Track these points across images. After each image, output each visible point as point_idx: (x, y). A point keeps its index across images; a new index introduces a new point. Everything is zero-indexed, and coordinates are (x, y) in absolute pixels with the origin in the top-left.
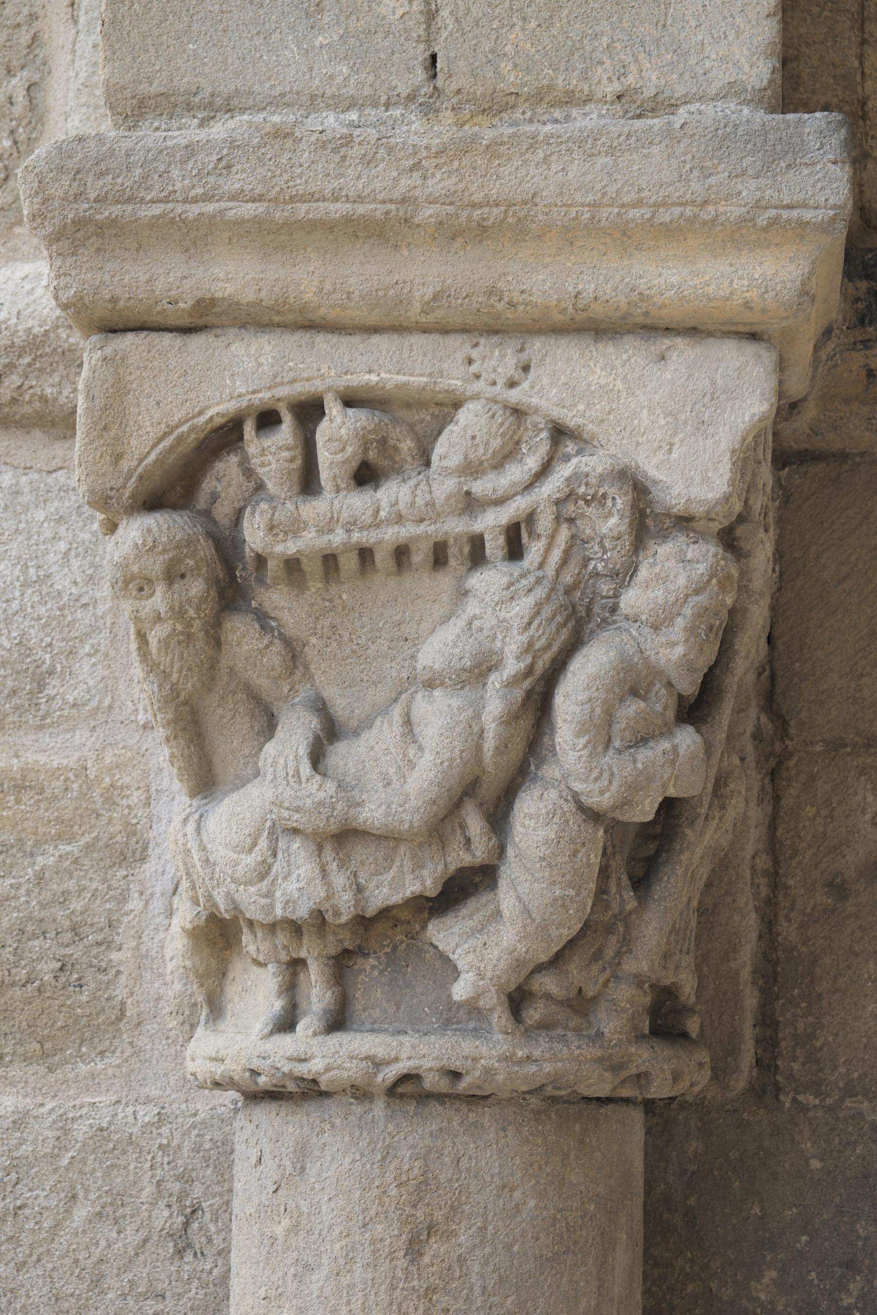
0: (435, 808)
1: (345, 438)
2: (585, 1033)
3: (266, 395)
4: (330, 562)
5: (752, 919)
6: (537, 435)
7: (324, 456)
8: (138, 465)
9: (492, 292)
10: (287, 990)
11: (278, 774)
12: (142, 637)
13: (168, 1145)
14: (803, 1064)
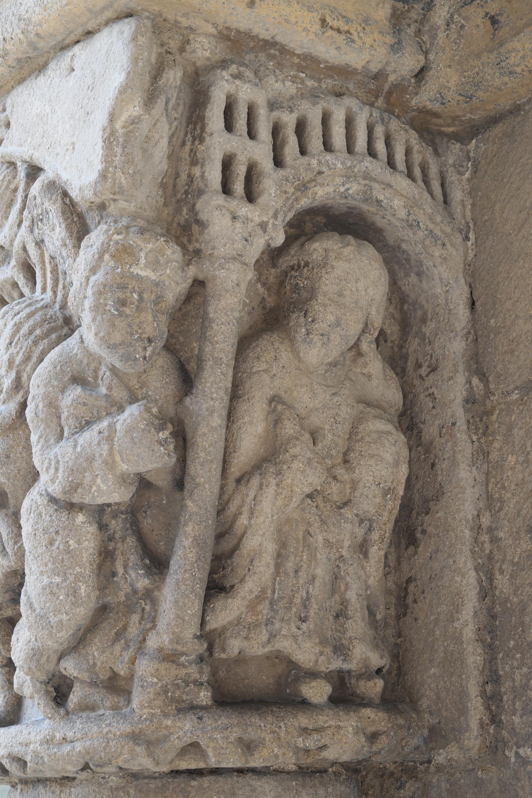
5: (472, 577)
14: (521, 717)
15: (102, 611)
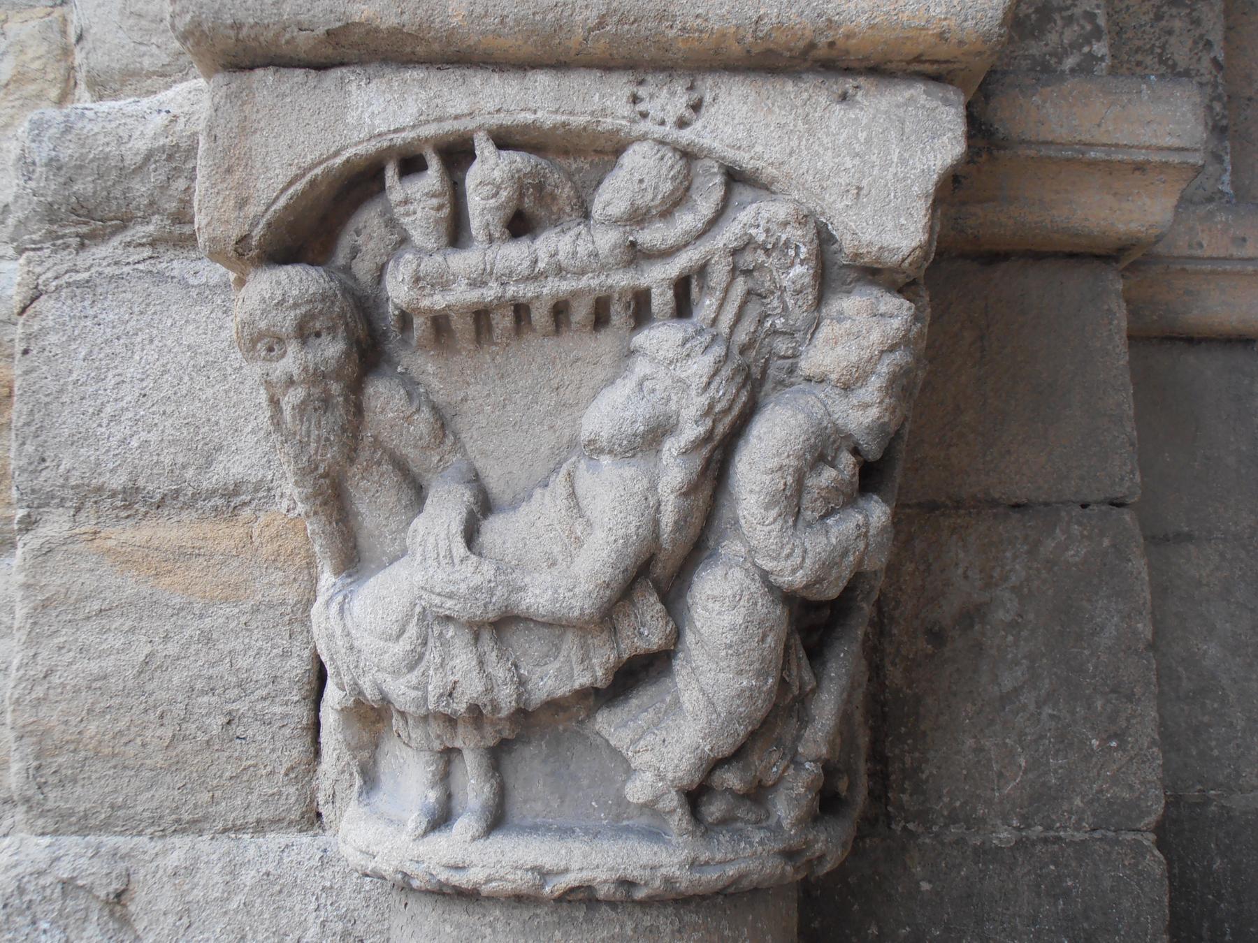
0: (608, 592)
1: (499, 180)
2: (764, 824)
3: (409, 135)
4: (481, 316)
6: (710, 181)
8: (266, 210)
10: (441, 780)
11: (425, 558)
12: (275, 402)
13: (331, 887)
14: (911, 795)
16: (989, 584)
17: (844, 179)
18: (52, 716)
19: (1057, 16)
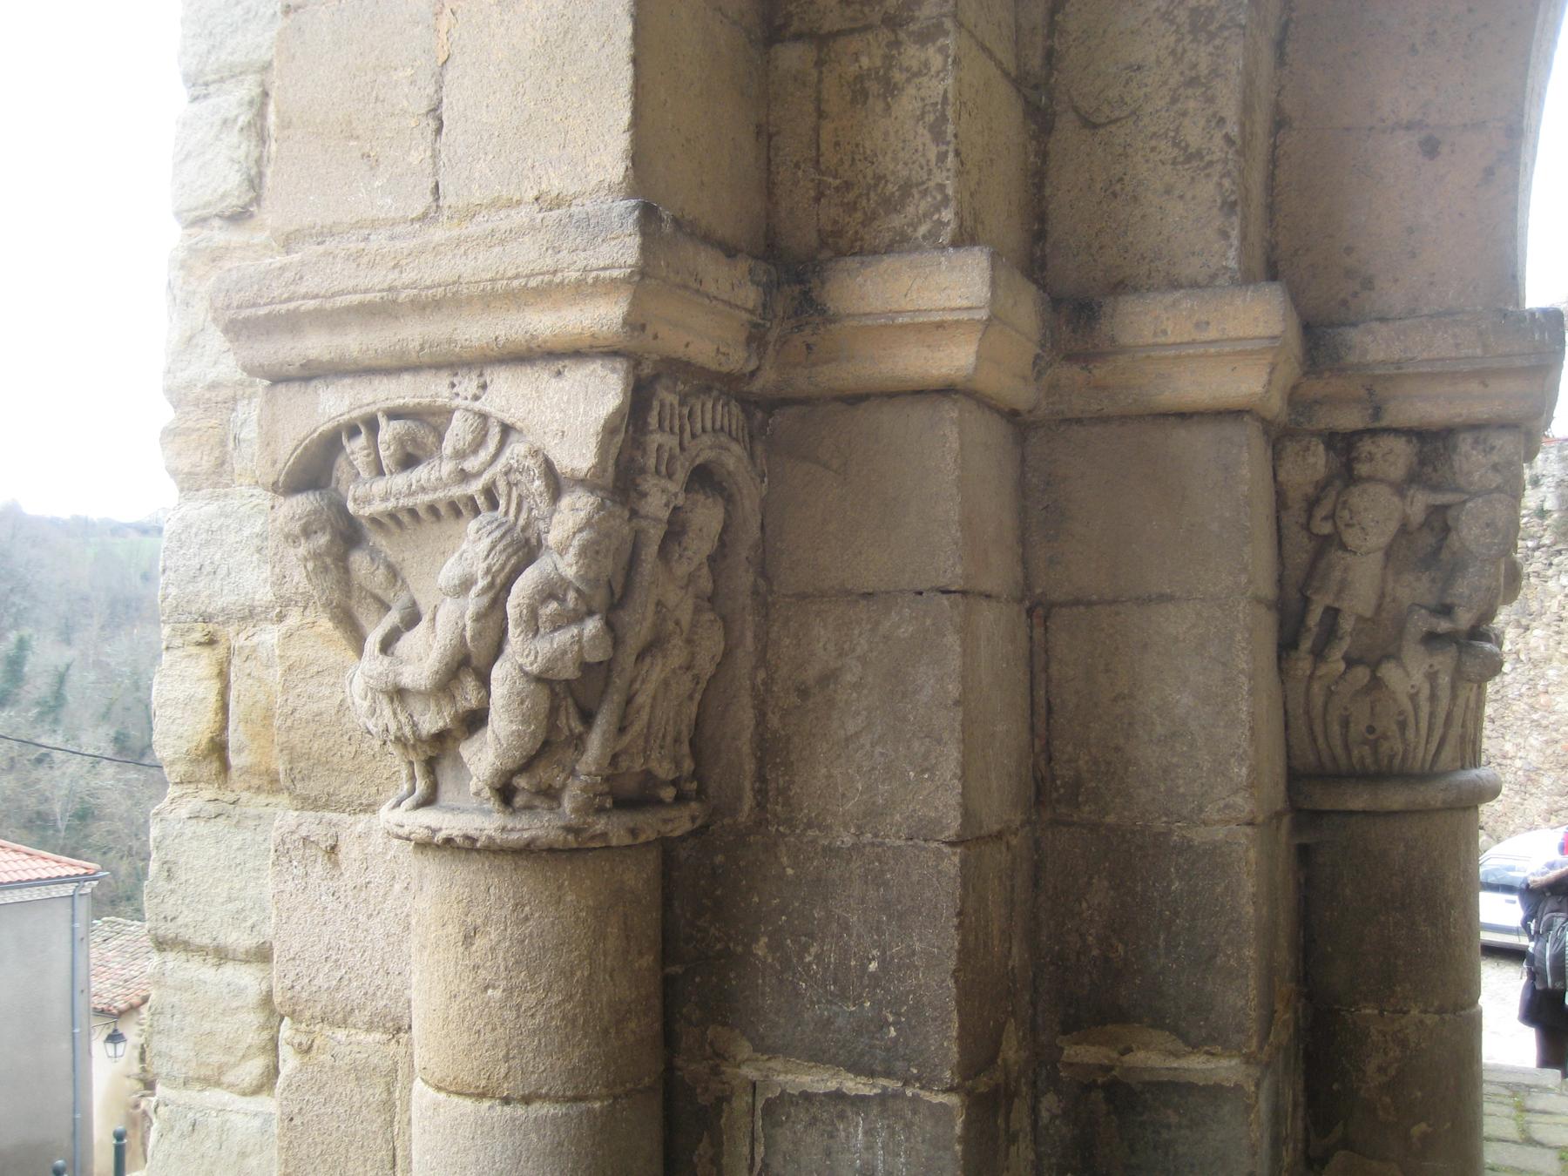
3: (346, 417)
7: (383, 453)
9: (450, 341)
15: (546, 744)
16: (842, 654)
17: (555, 426)
18: (295, 737)
19: (915, 191)
